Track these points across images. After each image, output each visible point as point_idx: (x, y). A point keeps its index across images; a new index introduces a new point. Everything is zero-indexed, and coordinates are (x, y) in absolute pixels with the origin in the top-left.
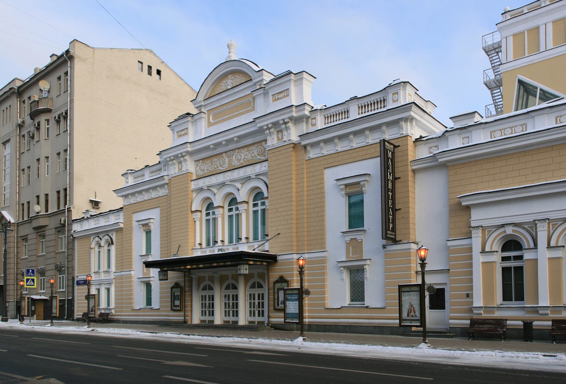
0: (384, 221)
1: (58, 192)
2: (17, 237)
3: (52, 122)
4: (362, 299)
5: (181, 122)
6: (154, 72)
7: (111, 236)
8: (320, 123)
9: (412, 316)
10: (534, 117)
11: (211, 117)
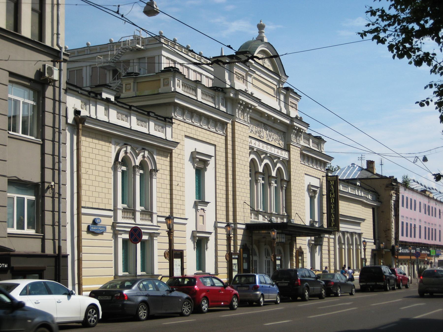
5: (142, 99)
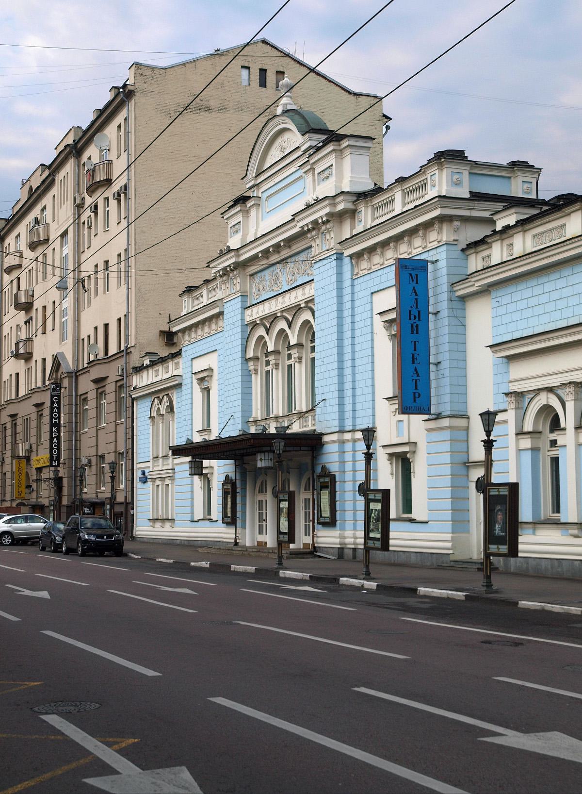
1: (119, 320)
2: (76, 396)
3: (113, 203)
4: (410, 512)
6: (271, 77)
8: (213, 551)
9: (280, 73)
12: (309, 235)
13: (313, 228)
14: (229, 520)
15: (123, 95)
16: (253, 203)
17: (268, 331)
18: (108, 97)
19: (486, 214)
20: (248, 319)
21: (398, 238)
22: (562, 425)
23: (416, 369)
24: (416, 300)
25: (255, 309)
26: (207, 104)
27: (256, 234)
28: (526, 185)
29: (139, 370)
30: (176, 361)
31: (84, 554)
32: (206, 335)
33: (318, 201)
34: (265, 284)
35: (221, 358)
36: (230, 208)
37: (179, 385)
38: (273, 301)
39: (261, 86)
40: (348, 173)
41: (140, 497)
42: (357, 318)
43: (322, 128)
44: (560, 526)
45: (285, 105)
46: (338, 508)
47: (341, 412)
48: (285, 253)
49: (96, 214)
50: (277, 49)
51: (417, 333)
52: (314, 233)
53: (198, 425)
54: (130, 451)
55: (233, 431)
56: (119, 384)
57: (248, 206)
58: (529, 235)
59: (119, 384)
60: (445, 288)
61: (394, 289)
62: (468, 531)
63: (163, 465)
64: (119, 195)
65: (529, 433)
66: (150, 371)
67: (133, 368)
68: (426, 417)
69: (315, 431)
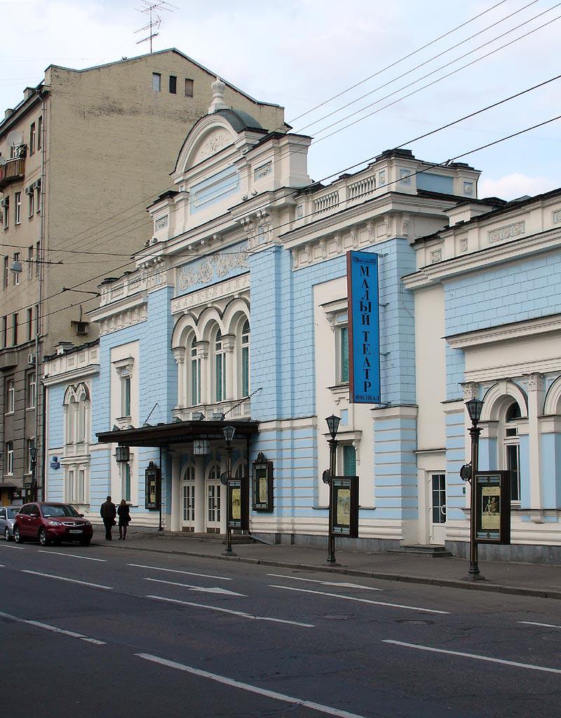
0: (347, 369)
1: (30, 310)
3: (25, 198)
6: (180, 85)
7: (523, 386)
10: (292, 530)
11: (187, 219)
12: (246, 228)
13: (251, 222)
14: (153, 506)
15: (38, 96)
16: (181, 197)
17: (197, 322)
18: (21, 97)
19: (440, 213)
20: (174, 310)
21: (344, 232)
22: (523, 414)
23: (367, 359)
24: (367, 291)
25: (183, 300)
26: (120, 107)
27: (184, 228)
28: (467, 186)
29: (51, 358)
30: (93, 350)
31: (47, 544)
32: (126, 326)
33: (256, 196)
34: (193, 275)
35: (143, 348)
36: (156, 202)
37: (97, 374)
38: (203, 293)
39: (171, 92)
40: (280, 171)
41: (50, 483)
42: (296, 310)
43: (256, 127)
44: (520, 512)
45: (216, 105)
46: (275, 495)
47: (279, 401)
48: (217, 246)
49: (7, 208)
50: (186, 59)
51: (368, 324)
52: (251, 226)
53: (117, 412)
54: (41, 438)
55: (160, 418)
56: (28, 372)
57: (176, 201)
58: (485, 231)
59: (28, 372)
60: (395, 280)
61: (345, 279)
62: (416, 518)
63: (67, 453)
64: (32, 190)
65: (487, 422)
66: (64, 360)
67: (45, 357)
68: (374, 406)
69: (250, 419)
